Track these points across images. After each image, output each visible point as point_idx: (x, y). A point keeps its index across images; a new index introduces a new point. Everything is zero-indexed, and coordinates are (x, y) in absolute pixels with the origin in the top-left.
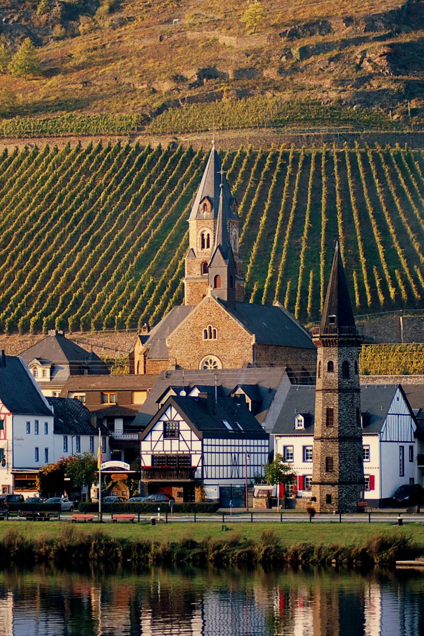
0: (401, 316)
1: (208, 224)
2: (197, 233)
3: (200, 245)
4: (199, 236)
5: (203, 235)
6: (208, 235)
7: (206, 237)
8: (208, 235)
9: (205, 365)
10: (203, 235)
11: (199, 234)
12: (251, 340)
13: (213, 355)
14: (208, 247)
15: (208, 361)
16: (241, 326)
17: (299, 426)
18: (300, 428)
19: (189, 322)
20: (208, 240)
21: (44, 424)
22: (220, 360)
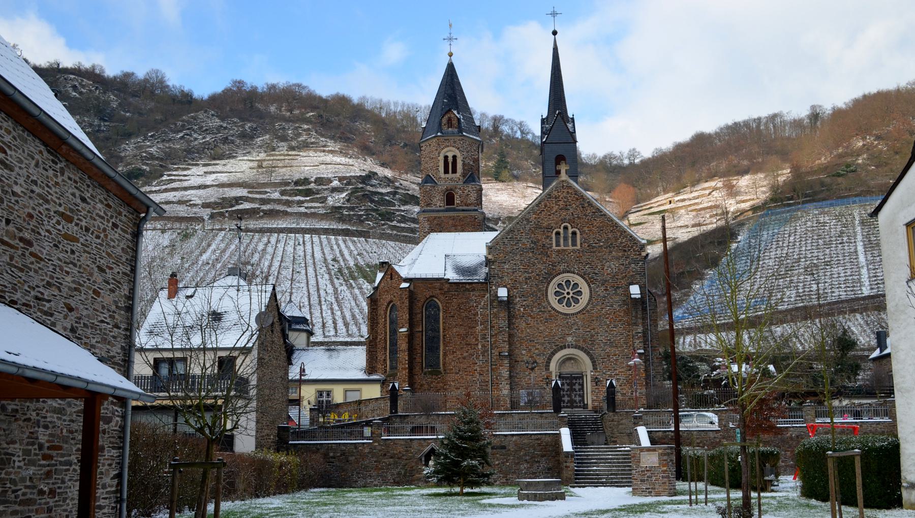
7: (450, 159)
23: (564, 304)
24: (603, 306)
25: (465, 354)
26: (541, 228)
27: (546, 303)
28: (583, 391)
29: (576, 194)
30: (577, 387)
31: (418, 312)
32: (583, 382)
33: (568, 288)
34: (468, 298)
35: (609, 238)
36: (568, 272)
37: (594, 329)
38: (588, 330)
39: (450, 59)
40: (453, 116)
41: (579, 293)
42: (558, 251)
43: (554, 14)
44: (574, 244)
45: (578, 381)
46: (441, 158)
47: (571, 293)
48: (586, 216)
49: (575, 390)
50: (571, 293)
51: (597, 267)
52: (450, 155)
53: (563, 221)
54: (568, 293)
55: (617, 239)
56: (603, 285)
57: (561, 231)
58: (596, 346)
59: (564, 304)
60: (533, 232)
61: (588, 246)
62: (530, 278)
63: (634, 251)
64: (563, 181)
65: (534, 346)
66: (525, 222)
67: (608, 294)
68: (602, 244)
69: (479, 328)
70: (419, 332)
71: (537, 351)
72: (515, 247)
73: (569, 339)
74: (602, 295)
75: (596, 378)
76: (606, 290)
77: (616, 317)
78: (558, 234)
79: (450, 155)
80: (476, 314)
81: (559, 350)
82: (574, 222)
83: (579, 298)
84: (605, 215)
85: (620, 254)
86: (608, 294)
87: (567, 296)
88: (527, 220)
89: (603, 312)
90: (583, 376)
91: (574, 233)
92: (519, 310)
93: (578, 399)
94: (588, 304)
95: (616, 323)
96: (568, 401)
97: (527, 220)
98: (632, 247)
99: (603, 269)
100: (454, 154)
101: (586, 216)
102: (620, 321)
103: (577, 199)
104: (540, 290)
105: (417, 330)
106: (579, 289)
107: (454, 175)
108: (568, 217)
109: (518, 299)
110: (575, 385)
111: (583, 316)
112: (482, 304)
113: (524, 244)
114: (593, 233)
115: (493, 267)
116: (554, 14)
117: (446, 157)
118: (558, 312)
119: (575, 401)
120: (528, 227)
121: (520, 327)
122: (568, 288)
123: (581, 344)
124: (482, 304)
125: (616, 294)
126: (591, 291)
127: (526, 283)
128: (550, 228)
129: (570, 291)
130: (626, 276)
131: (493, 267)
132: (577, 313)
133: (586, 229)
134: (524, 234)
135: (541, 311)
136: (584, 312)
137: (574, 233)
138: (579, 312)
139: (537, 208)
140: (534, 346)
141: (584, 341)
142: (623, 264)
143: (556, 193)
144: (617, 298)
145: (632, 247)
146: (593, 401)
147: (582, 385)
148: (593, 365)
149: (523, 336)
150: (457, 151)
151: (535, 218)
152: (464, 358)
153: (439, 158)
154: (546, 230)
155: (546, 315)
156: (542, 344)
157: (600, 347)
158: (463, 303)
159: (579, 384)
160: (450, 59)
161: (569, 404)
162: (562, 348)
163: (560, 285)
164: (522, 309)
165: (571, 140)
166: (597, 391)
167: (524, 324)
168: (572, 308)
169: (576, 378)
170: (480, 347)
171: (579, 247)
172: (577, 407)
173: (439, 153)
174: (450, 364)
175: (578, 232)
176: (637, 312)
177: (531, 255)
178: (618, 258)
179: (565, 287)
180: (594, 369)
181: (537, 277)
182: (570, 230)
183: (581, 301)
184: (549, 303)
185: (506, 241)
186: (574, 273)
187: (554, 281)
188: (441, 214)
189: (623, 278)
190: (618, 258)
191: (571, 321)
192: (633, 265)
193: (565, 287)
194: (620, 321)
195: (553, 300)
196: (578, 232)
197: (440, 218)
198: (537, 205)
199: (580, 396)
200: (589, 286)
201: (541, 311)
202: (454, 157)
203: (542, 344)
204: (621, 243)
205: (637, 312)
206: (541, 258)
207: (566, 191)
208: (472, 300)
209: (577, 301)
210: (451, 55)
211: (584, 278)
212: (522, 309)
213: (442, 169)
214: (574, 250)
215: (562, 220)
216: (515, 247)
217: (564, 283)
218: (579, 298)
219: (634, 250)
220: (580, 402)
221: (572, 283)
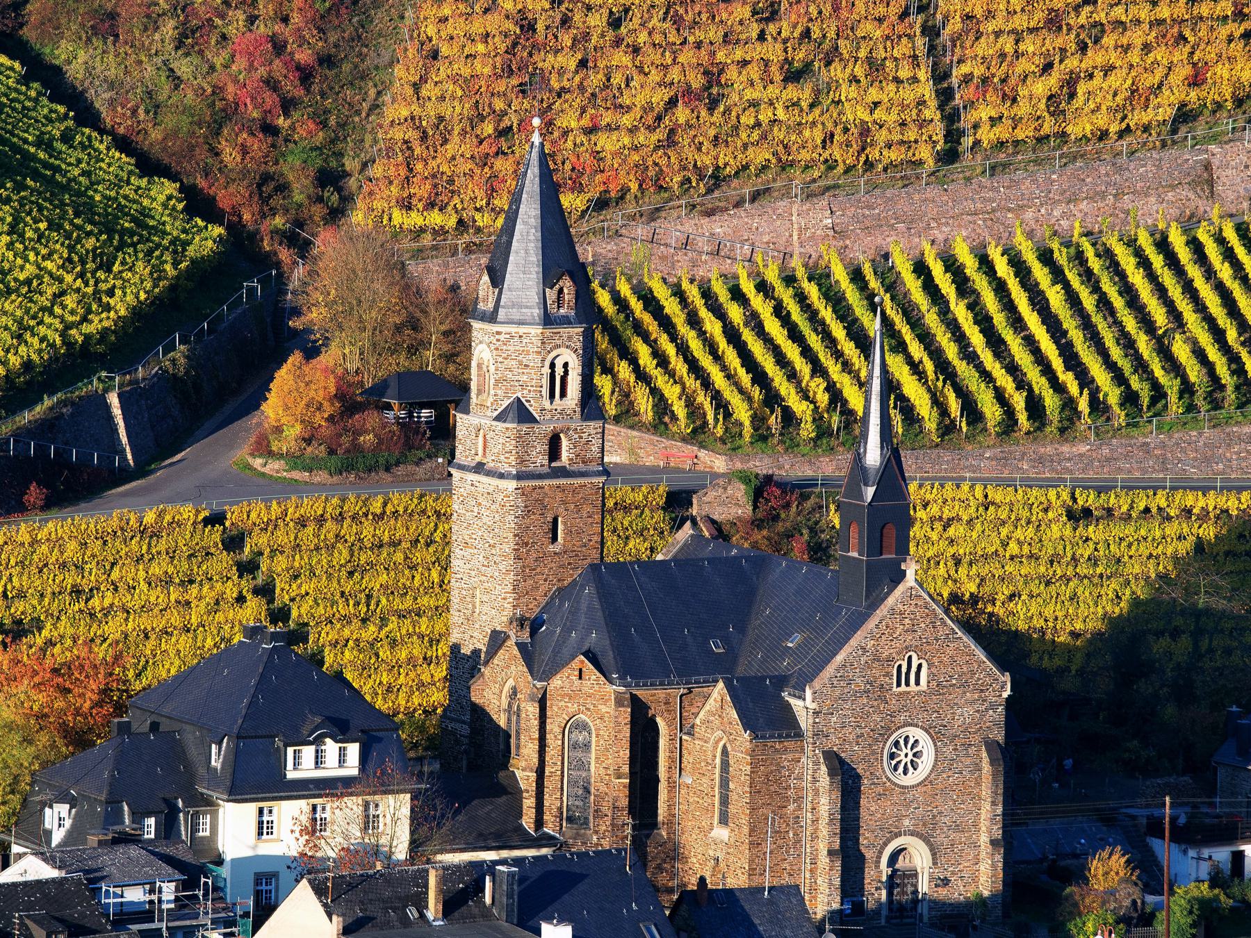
0: (53, 443)
1: (570, 338)
2: (543, 361)
3: (545, 391)
4: (547, 370)
5: (552, 366)
6: (566, 365)
7: (559, 371)
8: (566, 365)
9: (894, 750)
10: (552, 366)
11: (547, 364)
12: (1002, 688)
13: (917, 726)
14: (563, 394)
15: (911, 741)
16: (981, 655)
17: (268, 833)
18: (149, 836)
19: (862, 648)
20: (564, 379)
21: (276, 870)
22: (932, 737)
24: (950, 773)
33: (901, 750)
34: (778, 764)
36: (911, 725)
38: (930, 808)
45: (910, 881)
48: (937, 640)
53: (908, 649)
61: (938, 685)
62: (862, 735)
66: (860, 652)
68: (954, 682)
69: (791, 807)
76: (955, 750)
77: (965, 788)
91: (920, 666)
101: (937, 640)
104: (874, 753)
107: (918, 688)
111: (924, 789)
122: (901, 750)
125: (967, 755)
126: (936, 751)
127: (858, 744)
135: (874, 784)
137: (920, 666)
143: (900, 606)
155: (880, 789)
158: (772, 772)
159: (912, 885)
164: (850, 782)
170: (791, 835)
177: (865, 701)
178: (974, 702)
188: (546, 483)
192: (991, 712)
195: (912, 778)
197: (541, 488)
201: (874, 784)
204: (979, 679)
208: (784, 767)
211: (929, 733)
212: (850, 782)
215: (906, 648)
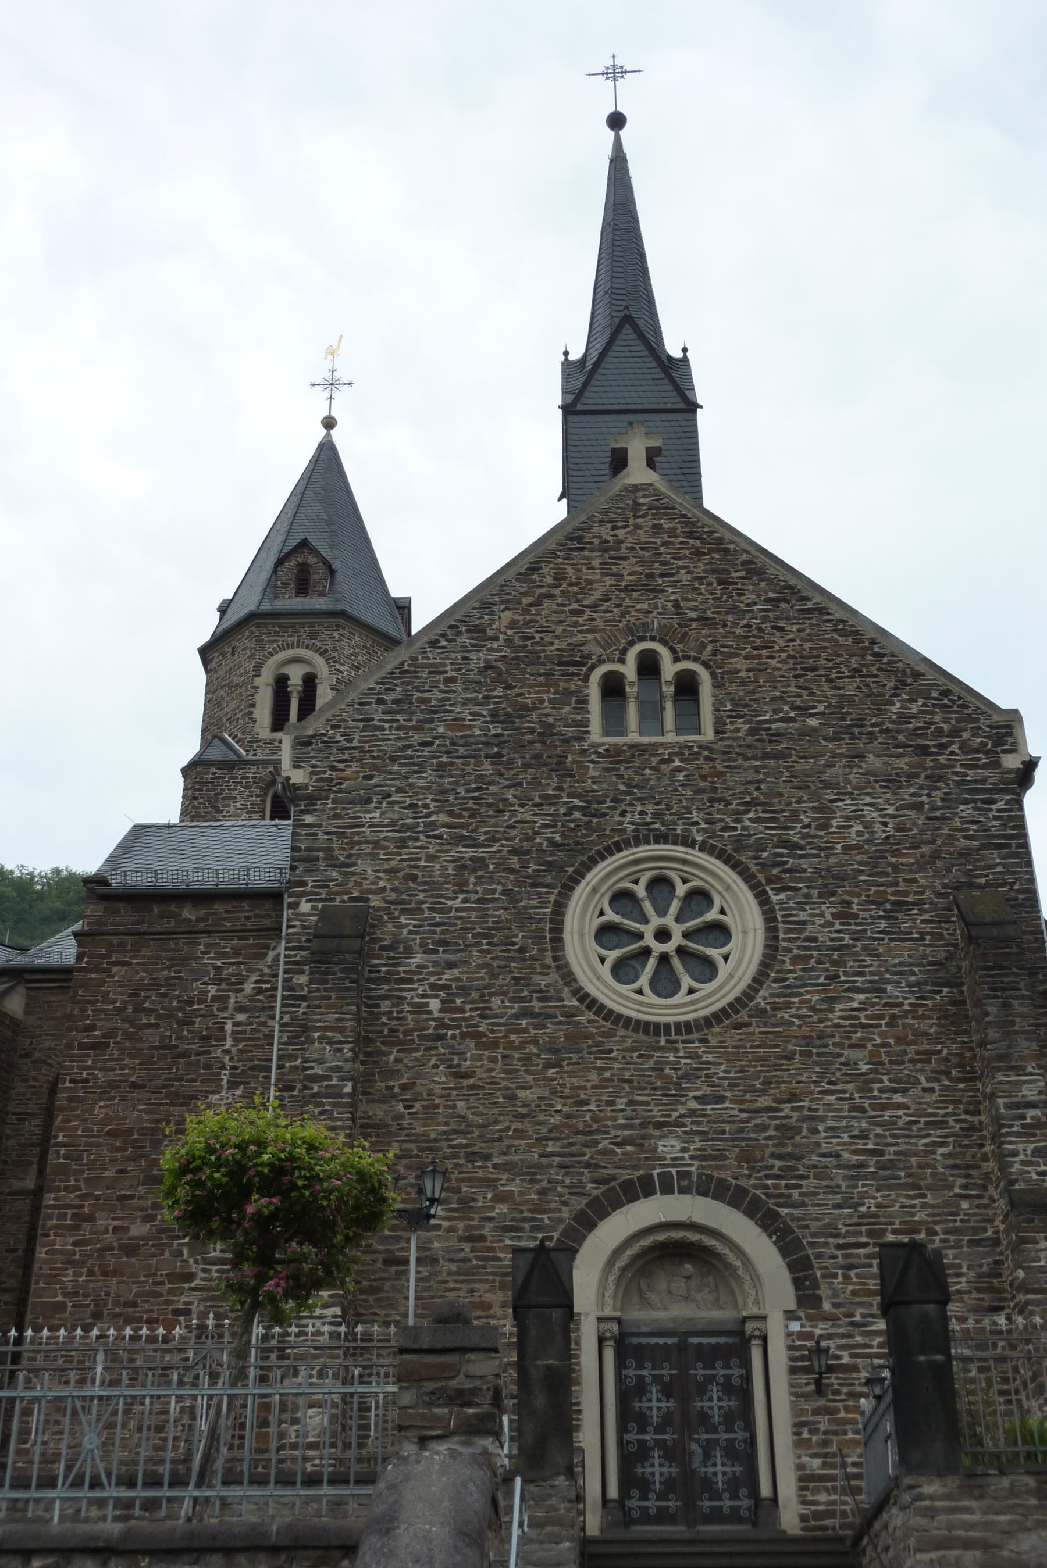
23: (644, 981)
25: (139, 1229)
26: (537, 662)
27: (554, 977)
28: (750, 1426)
29: (691, 535)
30: (715, 1403)
31: (32, 1107)
32: (748, 1378)
33: (662, 912)
35: (844, 700)
36: (661, 838)
37: (794, 1097)
38: (764, 1102)
39: (328, 435)
40: (312, 560)
41: (719, 932)
42: (614, 754)
43: (615, 73)
44: (689, 720)
46: (266, 679)
47: (677, 931)
49: (704, 1417)
50: (677, 931)
51: (795, 816)
52: (296, 675)
53: (636, 634)
54: (663, 935)
55: (880, 705)
56: (827, 893)
57: (629, 670)
58: (810, 1184)
59: (644, 981)
60: (500, 678)
61: (752, 732)
62: (480, 863)
63: (965, 747)
64: (635, 488)
65: (490, 1183)
66: (465, 640)
67: (857, 936)
68: (813, 722)
70: (23, 1193)
71: (502, 1208)
72: (416, 738)
73: (669, 1147)
74: (824, 937)
75: (819, 1351)
77: (899, 1040)
78: (613, 687)
79: (296, 675)
80: (214, 1036)
81: (617, 1205)
82: (684, 638)
83: (715, 953)
84: (822, 611)
85: (902, 764)
86: (857, 936)
87: (658, 948)
88: (478, 631)
89: (835, 1017)
90: (745, 1343)
92: (420, 1009)
93: (720, 1470)
94: (758, 980)
95: (906, 1069)
96: (670, 1486)
97: (478, 631)
98: (955, 733)
99: (825, 826)
100: (307, 669)
102: (925, 1057)
103: (698, 553)
104: (523, 918)
105: (17, 1185)
106: (712, 915)
108: (655, 621)
109: (418, 958)
110: (702, 1390)
112: (249, 987)
113: (457, 723)
114: (773, 682)
115: (309, 819)
116: (615, 73)
117: (281, 682)
118: (609, 1015)
119: (707, 1484)
120: (479, 659)
121: (422, 1086)
122: (662, 912)
123: (730, 1172)
124: (249, 987)
126: (770, 919)
127: (462, 887)
128: (582, 664)
129: (669, 921)
130: (936, 855)
131: (309, 819)
132: (708, 1022)
133: (739, 663)
134: (458, 687)
136: (743, 1016)
138: (718, 1017)
139: (522, 587)
140: (490, 1183)
141: (747, 1157)
142: (918, 807)
144: (904, 954)
145: (955, 733)
146: (806, 1479)
147: (745, 1394)
148: (798, 1284)
149: (434, 1131)
150: (319, 661)
151: (512, 625)
152: (131, 1250)
153: (257, 681)
154: (558, 670)
156: (531, 1172)
157: (834, 1190)
158: (155, 985)
160: (328, 435)
161: (672, 1504)
162: (644, 1188)
163: (622, 898)
164: (435, 1005)
165: (673, 401)
166: (823, 1423)
167: (441, 1077)
168: (680, 998)
169: (708, 1356)
171: (708, 734)
172: (716, 1516)
173: (258, 668)
174: (53, 1278)
175: (704, 676)
176: (1006, 1005)
177: (487, 768)
179: (648, 906)
180: (801, 1301)
181: (515, 862)
182: (669, 669)
183: (723, 969)
184: (568, 977)
185: (377, 713)
186: (687, 842)
187: (594, 876)
189: (921, 866)
190: (892, 782)
191: (678, 1059)
192: (966, 811)
193: (648, 906)
194: (925, 1057)
196: (704, 676)
198: (523, 577)
199: (731, 1452)
200: (763, 899)
202: (310, 682)
203: (531, 1172)
204: (904, 718)
205: (1006, 1005)
206: (535, 783)
207: (647, 522)
209: (706, 969)
210: (329, 423)
211: (735, 866)
213: (263, 713)
214: (684, 746)
215: (630, 630)
216: (416, 738)
217: (640, 890)
218: (715, 953)
219: (965, 747)
220: (733, 1486)
221: (681, 890)
